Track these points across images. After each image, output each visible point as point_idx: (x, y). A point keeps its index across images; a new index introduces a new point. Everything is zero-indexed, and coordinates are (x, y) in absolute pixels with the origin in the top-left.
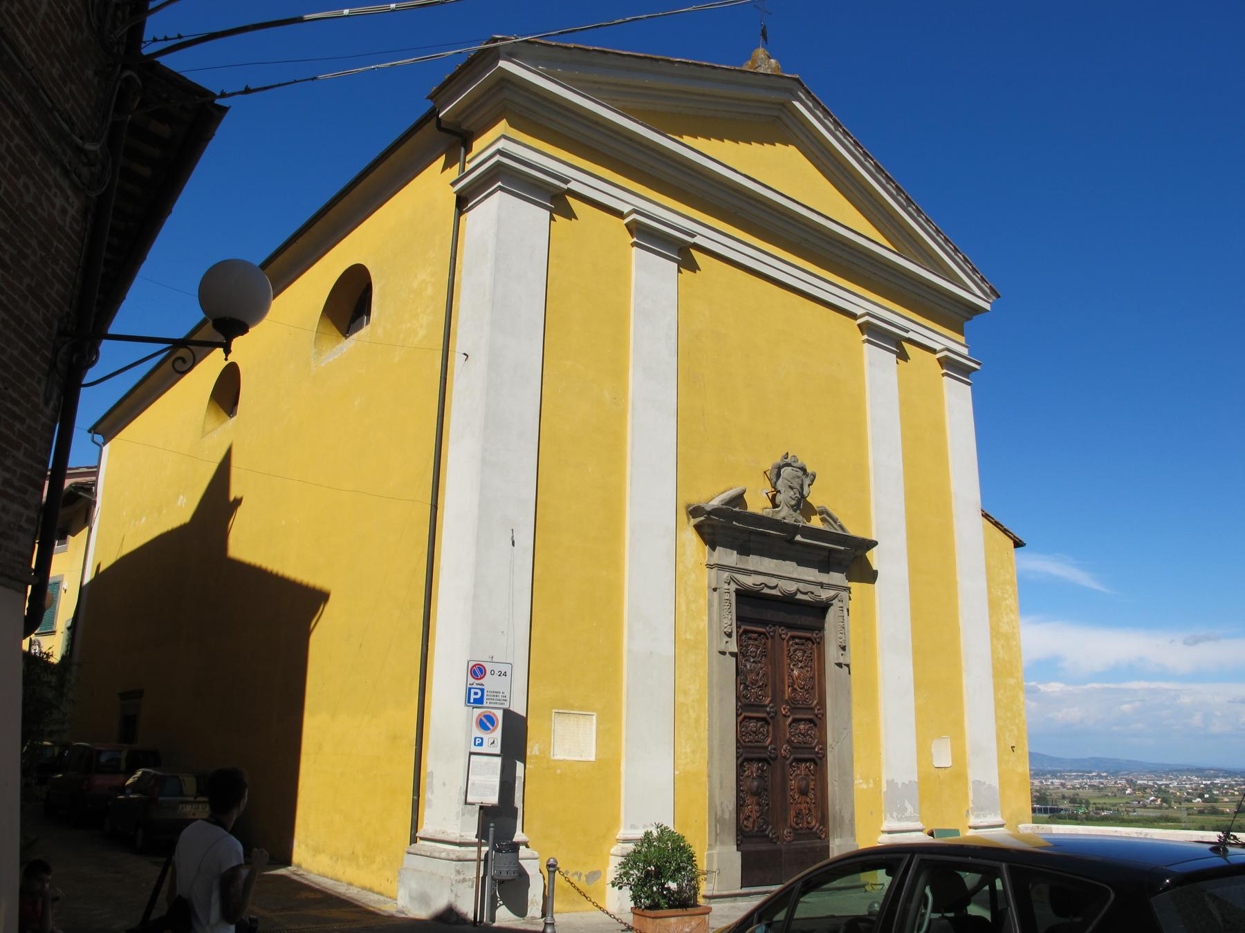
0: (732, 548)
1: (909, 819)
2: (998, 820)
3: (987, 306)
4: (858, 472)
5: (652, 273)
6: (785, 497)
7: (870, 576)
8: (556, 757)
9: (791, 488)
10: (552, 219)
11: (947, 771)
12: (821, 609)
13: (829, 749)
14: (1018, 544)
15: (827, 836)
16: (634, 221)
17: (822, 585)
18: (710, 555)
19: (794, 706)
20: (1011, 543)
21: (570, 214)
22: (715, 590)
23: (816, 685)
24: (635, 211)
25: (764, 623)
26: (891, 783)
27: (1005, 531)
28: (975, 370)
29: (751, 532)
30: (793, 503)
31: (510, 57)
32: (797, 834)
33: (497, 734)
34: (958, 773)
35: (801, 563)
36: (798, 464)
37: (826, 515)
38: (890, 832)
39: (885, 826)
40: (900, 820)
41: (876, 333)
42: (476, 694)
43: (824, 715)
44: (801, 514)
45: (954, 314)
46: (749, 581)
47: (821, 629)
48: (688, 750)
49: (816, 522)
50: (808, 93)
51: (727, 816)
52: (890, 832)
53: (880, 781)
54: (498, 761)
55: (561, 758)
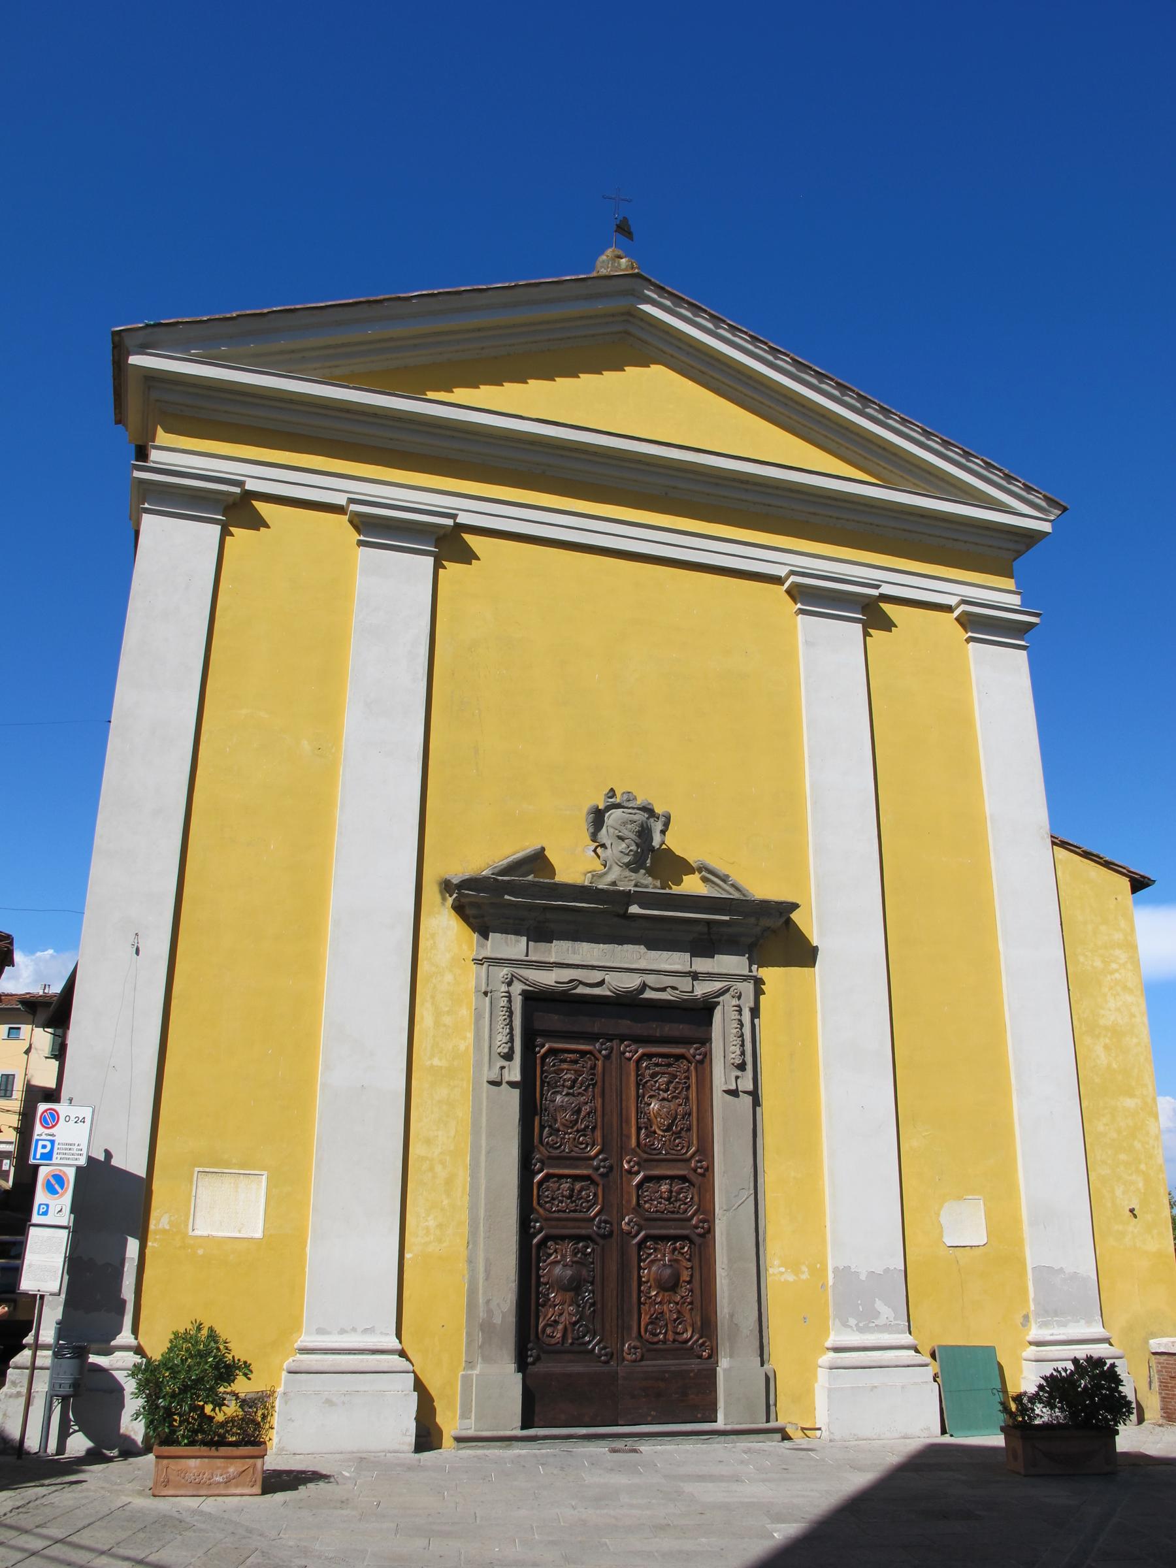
0: (517, 933)
1: (886, 1328)
2: (1097, 1330)
3: (1046, 527)
4: (786, 805)
5: (830, 650)
6: (617, 851)
7: (802, 953)
8: (198, 1233)
9: (621, 838)
10: (866, 634)
11: (977, 1252)
13: (717, 1221)
14: (1139, 884)
15: (713, 1355)
16: (964, 613)
17: (695, 976)
18: (481, 946)
19: (649, 1157)
20: (1125, 883)
21: (887, 624)
22: (486, 994)
23: (693, 1127)
24: (792, 573)
25: (592, 1038)
26: (843, 1273)
27: (1107, 865)
28: (1032, 625)
29: (546, 908)
30: (627, 859)
31: (142, 349)
32: (651, 1350)
33: (66, 1199)
34: (1003, 1252)
35: (652, 945)
37: (708, 873)
38: (837, 1350)
39: (833, 1340)
40: (861, 1330)
41: (813, 597)
42: (44, 1147)
43: (709, 1170)
44: (650, 872)
45: (995, 549)
46: (548, 979)
47: (706, 1040)
48: (431, 1223)
49: (691, 885)
50: (660, 289)
51: (498, 1320)
52: (837, 1350)
54: (64, 1234)
55: (205, 1234)
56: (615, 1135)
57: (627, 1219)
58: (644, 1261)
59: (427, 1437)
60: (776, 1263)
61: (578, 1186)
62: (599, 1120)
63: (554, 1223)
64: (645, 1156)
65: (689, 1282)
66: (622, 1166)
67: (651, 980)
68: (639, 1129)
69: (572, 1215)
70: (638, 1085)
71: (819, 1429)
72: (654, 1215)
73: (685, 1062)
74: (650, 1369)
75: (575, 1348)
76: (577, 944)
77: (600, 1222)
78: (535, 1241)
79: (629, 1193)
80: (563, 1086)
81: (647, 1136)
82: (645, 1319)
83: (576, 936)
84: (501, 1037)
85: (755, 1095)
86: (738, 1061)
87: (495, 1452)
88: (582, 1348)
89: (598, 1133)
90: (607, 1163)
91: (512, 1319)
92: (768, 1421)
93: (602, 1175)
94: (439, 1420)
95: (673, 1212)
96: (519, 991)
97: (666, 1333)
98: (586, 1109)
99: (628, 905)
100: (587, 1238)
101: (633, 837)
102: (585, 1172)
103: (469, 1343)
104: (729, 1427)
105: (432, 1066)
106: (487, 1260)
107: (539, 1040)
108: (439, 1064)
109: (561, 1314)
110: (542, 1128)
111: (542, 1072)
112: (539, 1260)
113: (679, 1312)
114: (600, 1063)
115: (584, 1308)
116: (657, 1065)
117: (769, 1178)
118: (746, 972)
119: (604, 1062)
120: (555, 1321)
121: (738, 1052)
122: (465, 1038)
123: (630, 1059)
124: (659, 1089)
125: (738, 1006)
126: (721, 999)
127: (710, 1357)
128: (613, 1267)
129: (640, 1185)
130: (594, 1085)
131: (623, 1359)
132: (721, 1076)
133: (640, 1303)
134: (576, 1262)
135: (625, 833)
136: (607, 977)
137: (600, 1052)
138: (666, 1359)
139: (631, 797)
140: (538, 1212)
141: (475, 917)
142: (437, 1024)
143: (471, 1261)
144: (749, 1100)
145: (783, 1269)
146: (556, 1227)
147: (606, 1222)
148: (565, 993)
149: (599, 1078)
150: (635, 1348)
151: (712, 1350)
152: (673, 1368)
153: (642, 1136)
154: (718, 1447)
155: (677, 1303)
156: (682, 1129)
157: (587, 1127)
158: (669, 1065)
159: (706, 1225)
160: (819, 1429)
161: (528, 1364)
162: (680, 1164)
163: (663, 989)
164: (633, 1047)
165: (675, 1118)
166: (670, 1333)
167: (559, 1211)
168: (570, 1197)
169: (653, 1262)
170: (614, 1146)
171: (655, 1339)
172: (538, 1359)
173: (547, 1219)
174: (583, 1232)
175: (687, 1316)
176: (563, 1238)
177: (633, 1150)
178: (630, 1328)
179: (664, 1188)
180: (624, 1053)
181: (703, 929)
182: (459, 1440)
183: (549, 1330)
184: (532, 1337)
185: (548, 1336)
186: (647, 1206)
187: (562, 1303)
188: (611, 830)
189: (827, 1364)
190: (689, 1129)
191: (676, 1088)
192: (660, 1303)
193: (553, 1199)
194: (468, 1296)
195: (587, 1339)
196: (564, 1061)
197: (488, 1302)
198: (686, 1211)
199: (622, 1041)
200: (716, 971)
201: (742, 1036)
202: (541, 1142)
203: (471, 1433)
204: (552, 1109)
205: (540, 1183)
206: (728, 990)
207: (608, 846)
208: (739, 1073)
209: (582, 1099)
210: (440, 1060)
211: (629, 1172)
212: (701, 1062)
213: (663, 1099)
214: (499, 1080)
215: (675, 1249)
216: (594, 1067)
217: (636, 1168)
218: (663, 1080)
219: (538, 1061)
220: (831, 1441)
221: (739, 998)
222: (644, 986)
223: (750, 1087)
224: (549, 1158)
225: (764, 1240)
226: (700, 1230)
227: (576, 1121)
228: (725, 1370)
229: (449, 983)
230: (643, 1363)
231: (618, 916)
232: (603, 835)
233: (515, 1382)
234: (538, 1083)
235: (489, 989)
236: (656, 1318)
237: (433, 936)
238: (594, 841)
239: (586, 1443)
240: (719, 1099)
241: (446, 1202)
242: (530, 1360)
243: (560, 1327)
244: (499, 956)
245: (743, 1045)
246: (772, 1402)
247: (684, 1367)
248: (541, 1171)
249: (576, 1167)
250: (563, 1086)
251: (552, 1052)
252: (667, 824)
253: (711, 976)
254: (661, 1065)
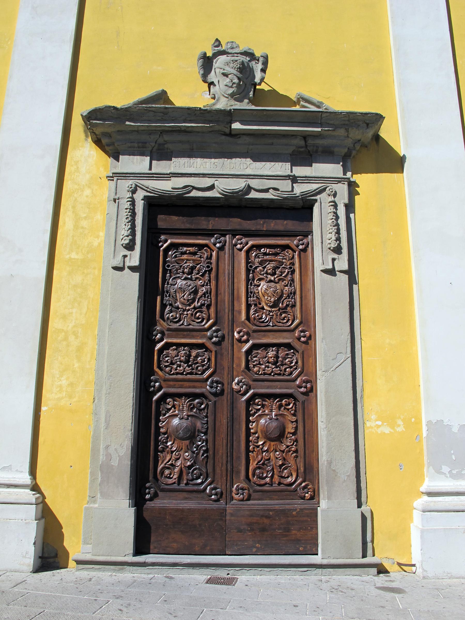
0: (142, 154)
6: (223, 85)
9: (225, 75)
12: (301, 210)
15: (315, 496)
17: (294, 179)
25: (209, 234)
26: (437, 427)
29: (163, 132)
30: (231, 91)
36: (242, 48)
38: (430, 494)
40: (454, 477)
46: (165, 186)
47: (308, 233)
48: (64, 382)
51: (115, 462)
52: (430, 494)
53: (419, 421)
56: (227, 310)
57: (236, 381)
58: (253, 415)
59: (50, 557)
60: (373, 417)
61: (194, 353)
62: (213, 299)
63: (171, 383)
65: (294, 434)
67: (254, 183)
68: (248, 306)
69: (189, 376)
71: (414, 565)
72: (262, 377)
73: (290, 251)
74: (256, 507)
75: (190, 487)
76: (192, 160)
77: (212, 382)
78: (155, 398)
79: (240, 359)
80: (183, 273)
81: (256, 311)
83: (191, 153)
84: (124, 231)
87: (106, 575)
89: (212, 310)
90: (220, 334)
91: (127, 463)
92: (364, 556)
93: (215, 343)
94: (66, 544)
95: (279, 374)
96: (142, 197)
97: (272, 477)
99: (231, 123)
100: (201, 395)
101: (235, 72)
102: (200, 341)
103: (93, 481)
104: (325, 562)
105: (70, 259)
106: (107, 412)
107: (163, 237)
108: (76, 257)
109: (177, 459)
110: (164, 306)
112: (158, 414)
113: (284, 459)
114: (214, 254)
115: (198, 454)
116: (265, 254)
117: (366, 343)
118: (341, 175)
119: (218, 253)
120: (172, 465)
121: (334, 238)
122: (98, 237)
125: (334, 202)
126: (318, 197)
127: (312, 498)
128: (223, 419)
129: (249, 352)
131: (232, 498)
132: (320, 258)
134: (192, 416)
135: (228, 70)
136: (216, 183)
137: (215, 245)
139: (233, 45)
141: (108, 145)
142: (76, 227)
143: (96, 413)
144: (345, 278)
145: (379, 423)
146: (173, 387)
147: (217, 382)
148: (180, 197)
149: (214, 266)
150: (243, 489)
151: (314, 491)
152: (277, 507)
153: (252, 312)
154: (314, 576)
155: (283, 452)
156: (287, 306)
157: (203, 305)
158: (276, 254)
160: (414, 565)
162: (285, 334)
163: (266, 191)
164: (244, 240)
165: (281, 296)
166: (276, 476)
167: (177, 374)
168: (187, 362)
169: (261, 416)
171: (263, 482)
172: (156, 495)
173: (165, 380)
174: (198, 391)
175: (291, 462)
176: (180, 395)
178: (239, 472)
179: (271, 353)
180: (236, 245)
181: (300, 142)
182: (79, 562)
183: (167, 472)
184: (151, 478)
185: (166, 477)
186: (256, 369)
188: (217, 71)
189: (420, 507)
190: (294, 306)
192: (267, 451)
193: (172, 363)
194: (93, 442)
195: (199, 481)
197: (107, 447)
198: (291, 374)
199: (234, 236)
200: (313, 175)
201: (337, 225)
202: (162, 317)
203: (88, 557)
206: (324, 190)
207: (216, 83)
208: (336, 256)
209: (200, 282)
210: (77, 253)
211: (239, 341)
212: (305, 250)
213: (270, 281)
214: (121, 265)
216: (210, 257)
217: (245, 337)
218: (270, 266)
219: (161, 253)
220: (424, 578)
221: (335, 195)
222: (249, 189)
223: (345, 267)
225: (362, 397)
226: (302, 390)
227: (193, 300)
228: (322, 511)
229: (87, 196)
230: (249, 502)
231: (225, 134)
232: (212, 77)
233: (128, 516)
234: (161, 270)
235: (117, 197)
236: (263, 464)
237: (77, 163)
238: (205, 81)
239: (191, 570)
241: (76, 365)
242: (148, 497)
243: (177, 470)
244: (125, 171)
245: (338, 232)
246: (369, 538)
247: (287, 507)
248: (161, 340)
249: (193, 337)
251: (173, 246)
252: (265, 63)
253: (307, 179)
254: (269, 254)
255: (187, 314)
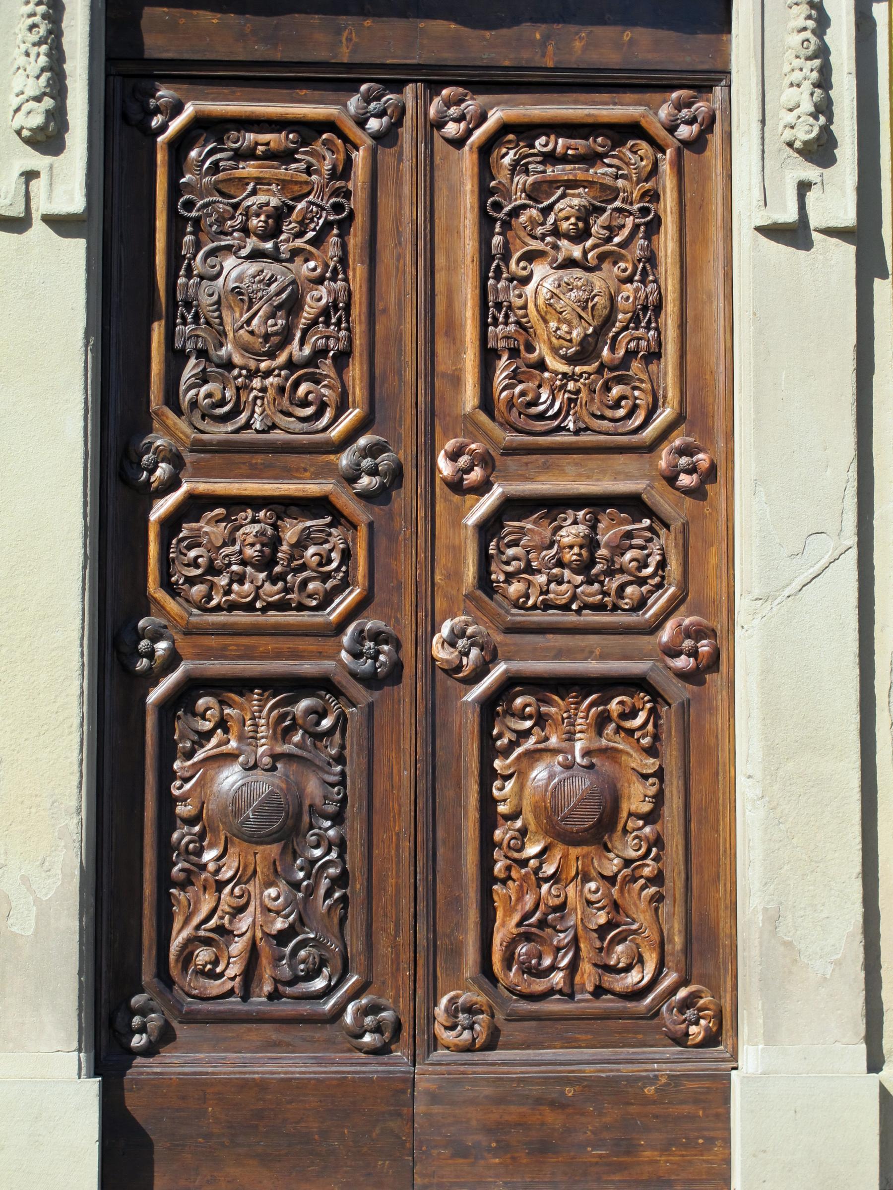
25: (338, 80)
47: (711, 78)
56: (409, 375)
57: (445, 630)
58: (506, 752)
61: (291, 531)
63: (213, 641)
64: (510, 438)
65: (650, 818)
66: (433, 467)
68: (488, 357)
69: (275, 617)
70: (486, 221)
73: (644, 147)
74: (518, 1072)
75: (285, 1007)
77: (360, 636)
78: (155, 695)
79: (457, 551)
81: (516, 377)
82: (505, 928)
85: (864, 236)
86: (807, 131)
88: (306, 1008)
89: (356, 371)
90: (384, 461)
93: (366, 496)
95: (599, 607)
97: (573, 968)
98: (318, 298)
100: (321, 685)
102: (313, 488)
107: (165, 93)
109: (241, 909)
110: (176, 358)
111: (175, 190)
112: (167, 751)
113: (616, 906)
115: (311, 891)
116: (550, 158)
120: (220, 930)
121: (807, 106)
123: (458, 143)
124: (556, 232)
127: (712, 1040)
128: (400, 770)
129: (489, 528)
130: (345, 225)
131: (434, 1043)
133: (487, 879)
134: (289, 757)
137: (361, 123)
138: (570, 1044)
140: (162, 610)
144: (845, 255)
146: (220, 654)
147: (377, 637)
149: (358, 203)
150: (470, 1010)
152: (589, 1070)
153: (500, 377)
155: (611, 880)
156: (631, 354)
157: (320, 353)
158: (591, 159)
159: (704, 647)
161: (133, 1053)
164: (471, 105)
165: (609, 320)
166: (586, 967)
167: (232, 607)
168: (267, 563)
169: (533, 756)
170: (404, 409)
171: (539, 985)
173: (189, 632)
174: (307, 668)
175: (641, 915)
176: (243, 685)
177: (468, 417)
178: (456, 952)
179: (571, 532)
183: (203, 955)
184: (148, 975)
186: (515, 588)
187: (242, 877)
190: (654, 355)
191: (612, 230)
192: (554, 878)
193: (213, 570)
196: (249, 154)
198: (641, 604)
199: (434, 87)
201: (823, 52)
202: (172, 399)
204: (206, 301)
205: (171, 525)
208: (811, 172)
209: (307, 268)
211: (456, 486)
212: (698, 144)
213: (570, 263)
214: (18, 211)
215: (603, 720)
216: (344, 171)
217: (477, 474)
218: (570, 204)
219: (161, 157)
223: (846, 214)
224: (199, 447)
226: (683, 662)
227: (286, 336)
236: (542, 924)
240: (754, 261)
242: (138, 1041)
243: (238, 946)
245: (824, 82)
247: (626, 1070)
248: (172, 484)
249: (287, 474)
250: (245, 231)
251: (205, 127)
254: (564, 159)
255: (264, 390)
